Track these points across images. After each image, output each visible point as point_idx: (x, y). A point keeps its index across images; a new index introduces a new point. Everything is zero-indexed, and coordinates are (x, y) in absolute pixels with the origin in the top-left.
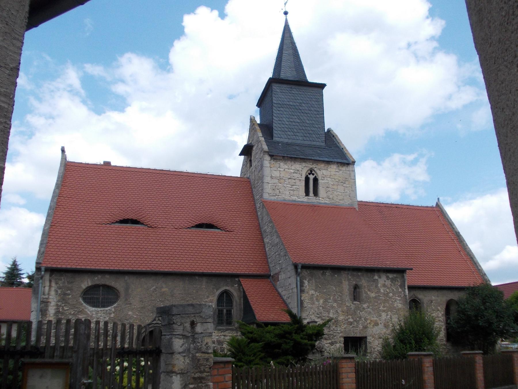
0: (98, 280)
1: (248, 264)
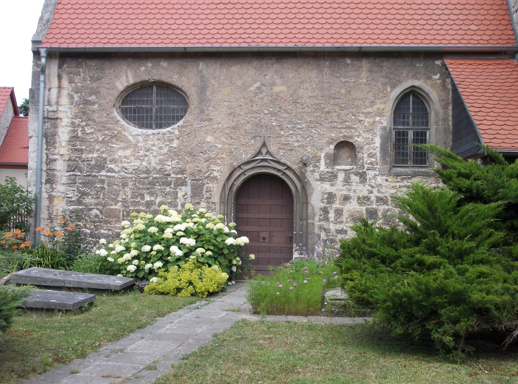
0: (148, 72)
1: (464, 27)
